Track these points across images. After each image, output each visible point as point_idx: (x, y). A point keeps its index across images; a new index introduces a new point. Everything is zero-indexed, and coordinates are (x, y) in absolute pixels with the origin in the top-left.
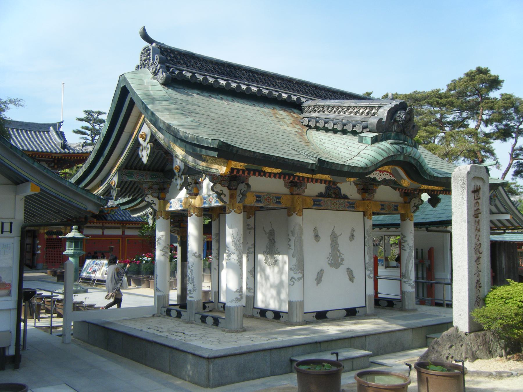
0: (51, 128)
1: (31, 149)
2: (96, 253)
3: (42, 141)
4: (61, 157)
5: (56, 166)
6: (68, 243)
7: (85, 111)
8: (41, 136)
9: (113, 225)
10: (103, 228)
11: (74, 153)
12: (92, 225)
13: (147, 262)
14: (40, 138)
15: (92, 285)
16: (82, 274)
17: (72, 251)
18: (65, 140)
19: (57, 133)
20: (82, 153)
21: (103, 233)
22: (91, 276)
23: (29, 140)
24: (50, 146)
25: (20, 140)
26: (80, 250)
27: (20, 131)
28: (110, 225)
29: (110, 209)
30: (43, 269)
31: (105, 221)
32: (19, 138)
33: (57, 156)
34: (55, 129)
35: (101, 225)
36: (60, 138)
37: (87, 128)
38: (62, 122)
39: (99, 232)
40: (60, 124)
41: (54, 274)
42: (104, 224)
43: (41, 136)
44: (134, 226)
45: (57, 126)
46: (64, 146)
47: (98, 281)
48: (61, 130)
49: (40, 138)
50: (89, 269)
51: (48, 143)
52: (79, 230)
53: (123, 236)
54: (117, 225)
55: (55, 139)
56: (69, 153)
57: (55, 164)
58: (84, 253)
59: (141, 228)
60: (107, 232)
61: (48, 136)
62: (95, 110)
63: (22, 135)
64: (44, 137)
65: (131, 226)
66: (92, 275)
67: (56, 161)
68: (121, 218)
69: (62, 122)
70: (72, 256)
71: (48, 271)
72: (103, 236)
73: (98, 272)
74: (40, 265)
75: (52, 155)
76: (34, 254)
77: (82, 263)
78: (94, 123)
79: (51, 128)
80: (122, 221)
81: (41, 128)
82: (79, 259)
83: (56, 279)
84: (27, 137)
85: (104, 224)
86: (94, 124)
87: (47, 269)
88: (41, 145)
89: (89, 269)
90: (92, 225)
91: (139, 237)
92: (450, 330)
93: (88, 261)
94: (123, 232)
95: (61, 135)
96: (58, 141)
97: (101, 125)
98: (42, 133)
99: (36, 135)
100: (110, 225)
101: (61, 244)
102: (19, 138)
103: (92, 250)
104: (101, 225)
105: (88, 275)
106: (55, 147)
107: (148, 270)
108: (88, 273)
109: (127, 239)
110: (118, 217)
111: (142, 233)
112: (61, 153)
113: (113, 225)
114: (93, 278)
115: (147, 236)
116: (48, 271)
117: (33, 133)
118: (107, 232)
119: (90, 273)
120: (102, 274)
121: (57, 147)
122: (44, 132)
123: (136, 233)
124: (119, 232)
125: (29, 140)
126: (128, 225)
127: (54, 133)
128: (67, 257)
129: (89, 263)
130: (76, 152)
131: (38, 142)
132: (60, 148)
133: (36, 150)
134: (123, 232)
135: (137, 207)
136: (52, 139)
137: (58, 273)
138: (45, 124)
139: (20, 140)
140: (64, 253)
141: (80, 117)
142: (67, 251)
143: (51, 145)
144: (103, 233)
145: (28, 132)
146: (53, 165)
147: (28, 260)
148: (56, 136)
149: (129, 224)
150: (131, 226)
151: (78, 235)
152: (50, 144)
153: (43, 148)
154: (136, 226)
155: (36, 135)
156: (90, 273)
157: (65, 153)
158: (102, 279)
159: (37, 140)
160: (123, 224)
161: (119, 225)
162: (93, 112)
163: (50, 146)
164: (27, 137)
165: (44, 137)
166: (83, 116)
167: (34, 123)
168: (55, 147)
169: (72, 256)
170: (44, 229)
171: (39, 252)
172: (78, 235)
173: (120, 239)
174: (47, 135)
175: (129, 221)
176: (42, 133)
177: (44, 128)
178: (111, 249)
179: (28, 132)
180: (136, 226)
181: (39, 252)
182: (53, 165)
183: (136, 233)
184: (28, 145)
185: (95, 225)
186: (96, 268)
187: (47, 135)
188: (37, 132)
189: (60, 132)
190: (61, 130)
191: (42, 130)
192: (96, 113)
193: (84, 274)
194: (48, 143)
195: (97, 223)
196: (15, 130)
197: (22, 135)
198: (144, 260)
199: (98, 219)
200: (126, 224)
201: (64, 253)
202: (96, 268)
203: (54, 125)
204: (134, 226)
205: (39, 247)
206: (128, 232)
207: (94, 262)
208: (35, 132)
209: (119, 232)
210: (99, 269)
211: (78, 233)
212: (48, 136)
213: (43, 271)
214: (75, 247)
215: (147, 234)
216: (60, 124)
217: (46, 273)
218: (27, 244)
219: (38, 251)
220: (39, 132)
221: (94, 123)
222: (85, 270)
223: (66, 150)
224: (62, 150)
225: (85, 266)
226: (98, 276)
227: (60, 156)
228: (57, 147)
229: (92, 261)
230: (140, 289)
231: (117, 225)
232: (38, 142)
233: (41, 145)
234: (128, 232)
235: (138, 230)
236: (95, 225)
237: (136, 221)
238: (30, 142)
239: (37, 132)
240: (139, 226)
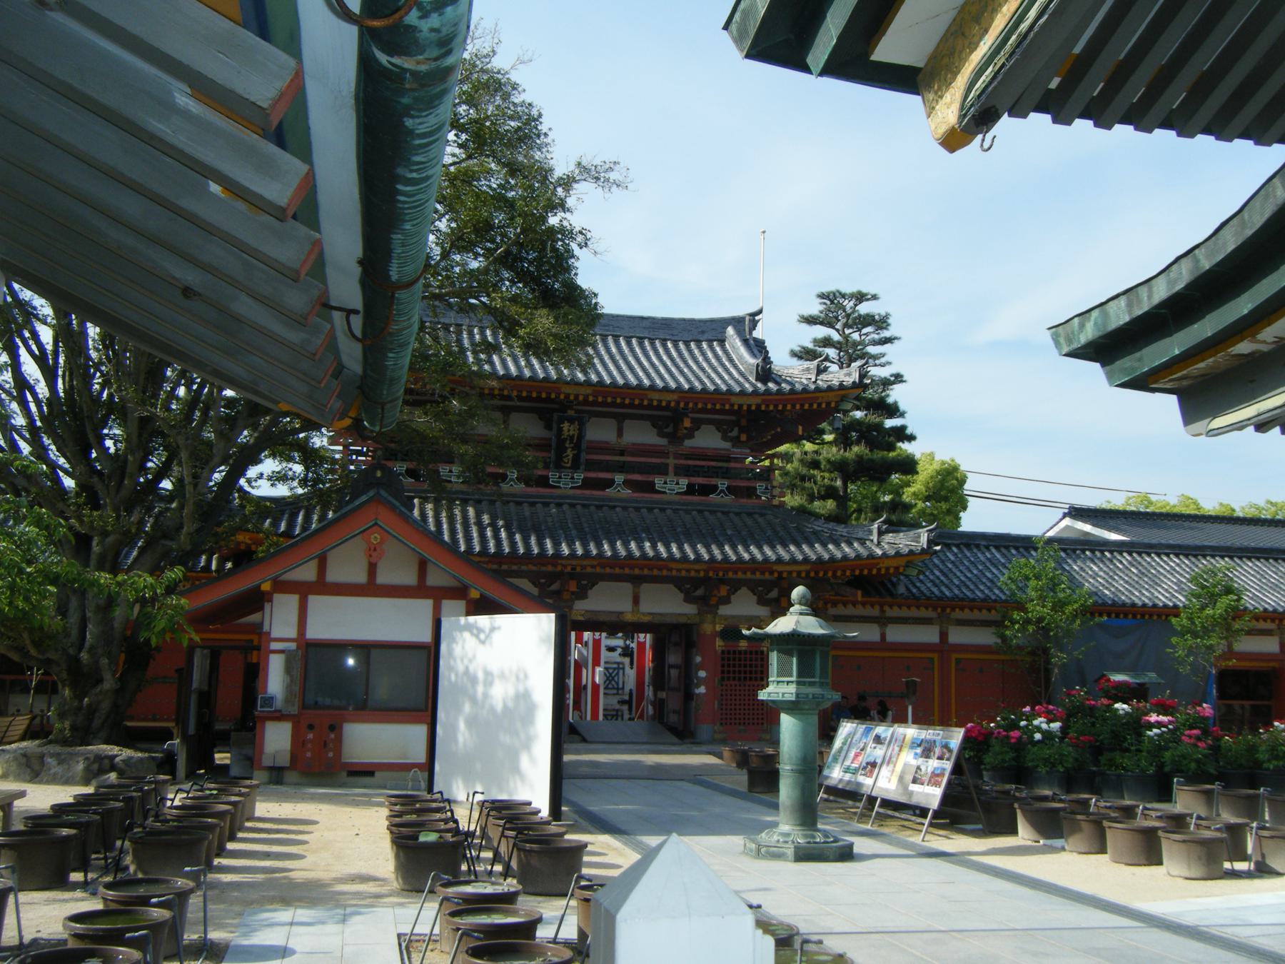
0: (730, 331)
1: (673, 385)
2: (862, 698)
3: (705, 365)
4: (758, 406)
5: (744, 437)
6: (774, 658)
7: (822, 296)
8: (704, 354)
9: (914, 613)
10: (883, 621)
11: (792, 391)
12: (850, 611)
13: (1048, 735)
14: (701, 359)
15: (863, 817)
16: (826, 772)
17: (792, 689)
18: (766, 360)
19: (746, 342)
20: (818, 389)
21: (883, 636)
22: (859, 785)
23: (669, 363)
24: (726, 377)
25: (646, 363)
26: (822, 685)
27: (647, 343)
28: (905, 612)
29: (902, 562)
30: (713, 741)
31: (889, 599)
32: (643, 359)
33: (744, 401)
34: (740, 333)
35: (875, 612)
36: (754, 356)
37: (827, 342)
38: (760, 312)
39: (870, 633)
40: (754, 317)
41: (743, 760)
42: (887, 608)
43: (704, 354)
44: (976, 615)
45: (745, 324)
46: (765, 373)
47: (886, 803)
48: (756, 334)
49: (701, 359)
50: (852, 754)
51: (720, 370)
52: (815, 608)
53: (943, 648)
54: (923, 613)
55: (741, 358)
56: (780, 392)
57: (741, 431)
58: (836, 696)
59: (998, 624)
60: (897, 634)
61: (720, 353)
62: (848, 289)
63: (651, 353)
64: (710, 355)
65: (967, 614)
66: (861, 779)
67: (744, 422)
68: (935, 590)
69: (760, 312)
70: (793, 707)
71: (726, 751)
72: (883, 644)
73: (885, 771)
74: (705, 730)
75: (734, 399)
76: (688, 696)
77: (827, 734)
78: (846, 325)
79: (730, 331)
80: (940, 599)
81: (703, 332)
82: (816, 718)
83: (743, 778)
84: (665, 358)
85: (887, 608)
86: (847, 331)
87: (724, 741)
88: (701, 374)
89: (852, 754)
90: (850, 611)
91: (997, 652)
92: (936, 718)
93: (846, 728)
94: (943, 636)
95: (758, 347)
96: (749, 361)
97: (864, 331)
98: (705, 345)
99: (690, 351)
100: (905, 612)
101: (747, 666)
102: (643, 359)
103: (865, 692)
104: (875, 612)
105: (848, 777)
106: (741, 380)
107: (1053, 765)
108: (847, 770)
109: (954, 656)
110: (927, 587)
111: (1004, 638)
112: (755, 393)
113: (914, 613)
114: (865, 790)
115: (1019, 647)
116: (726, 751)
117: (681, 345)
118: (897, 634)
119: (855, 772)
120: (901, 778)
121: (747, 380)
122: (710, 342)
123: (985, 637)
124: (929, 635)
125: (669, 363)
126: (958, 614)
127: (738, 343)
128: (770, 713)
129: (851, 735)
130: (799, 387)
131: (695, 368)
132: (752, 379)
133: (687, 386)
134: (943, 636)
135: (1244, 347)
136: (731, 360)
137: (755, 762)
138: (712, 321)
139: (646, 363)
140: (763, 695)
141: (806, 313)
142: (771, 688)
143: (730, 374)
144: (883, 636)
145: (669, 345)
146: (735, 433)
147: (674, 712)
148: (743, 350)
149: (962, 609)
150: (967, 614)
151: (812, 626)
152: (730, 369)
153: (706, 381)
154: (984, 615)
155: (690, 351)
156: (855, 772)
157: (768, 392)
158: (902, 799)
159: (691, 362)
160: (944, 610)
161: (930, 613)
162: (843, 296)
163: (726, 377)
164: (665, 358)
165: (710, 355)
166: (815, 308)
167: (684, 320)
168: (741, 380)
169: (793, 707)
170: (714, 623)
171: (702, 690)
172: (812, 626)
173: (935, 656)
174: (718, 349)
175: (962, 600)
176: (705, 345)
177: (707, 332)
178: (911, 686)
179: (669, 345)
180: (984, 615)
181: (702, 690)
182: (735, 433)
183: (985, 637)
184: (666, 376)
185: (859, 611)
186: (878, 753)
187: (718, 349)
188: (693, 345)
189: (755, 340)
190: (756, 334)
191: (706, 336)
192: (852, 296)
193: (836, 774)
194: (720, 370)
195: (864, 604)
196: (634, 341)
197: (651, 353)
198: (1039, 729)
199: (866, 593)
200: (953, 609)
201: (763, 695)
202: (878, 753)
203: (737, 322)
204: (976, 615)
205: (702, 674)
206: (958, 636)
207: (868, 731)
208: (687, 344)
209: (929, 635)
210: (887, 760)
211: (812, 619)
212: (720, 353)
213: (710, 748)
214: (800, 675)
215: (1021, 642)
216: (754, 317)
217: (720, 756)
218: (671, 666)
219: (698, 686)
220: (698, 342)
221: (846, 325)
222: (835, 759)
223: (771, 385)
224: (759, 385)
225: (837, 743)
226: (885, 784)
227: (754, 402)
228: (747, 380)
229: (862, 728)
230: (1064, 856)
231: (923, 613)
232: (695, 368)
233: (701, 374)
234: (958, 636)
235: (993, 629)
236: (859, 611)
237: (984, 600)
238: (673, 369)
239: (693, 345)
240: (994, 615)
